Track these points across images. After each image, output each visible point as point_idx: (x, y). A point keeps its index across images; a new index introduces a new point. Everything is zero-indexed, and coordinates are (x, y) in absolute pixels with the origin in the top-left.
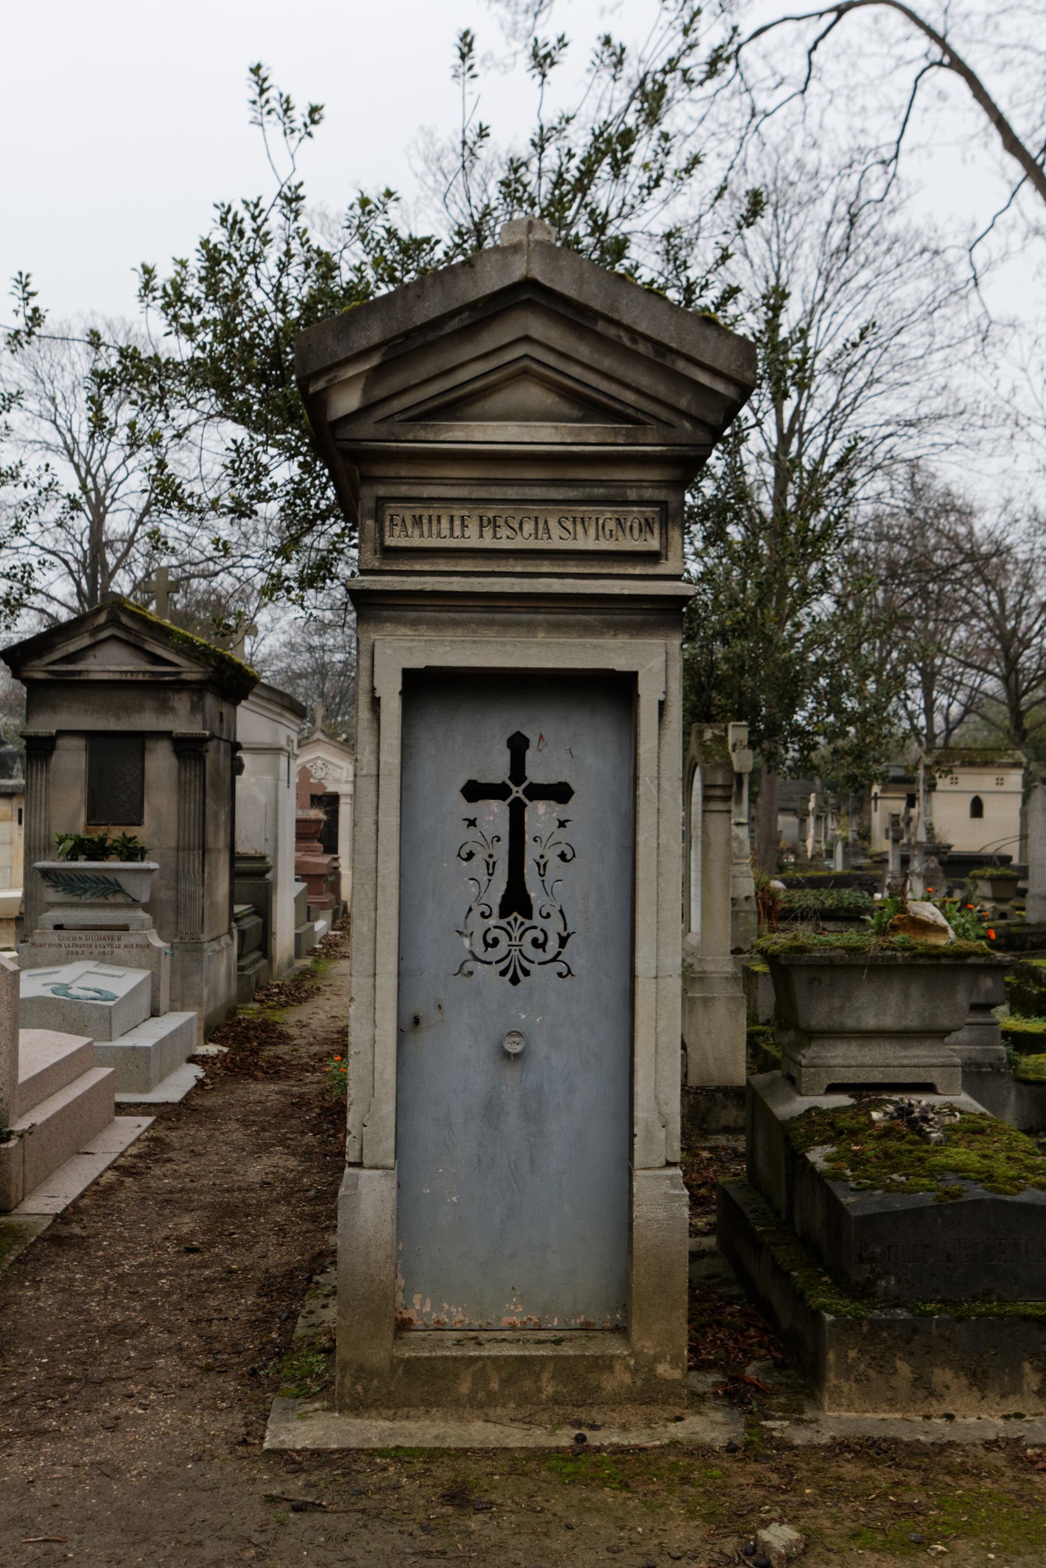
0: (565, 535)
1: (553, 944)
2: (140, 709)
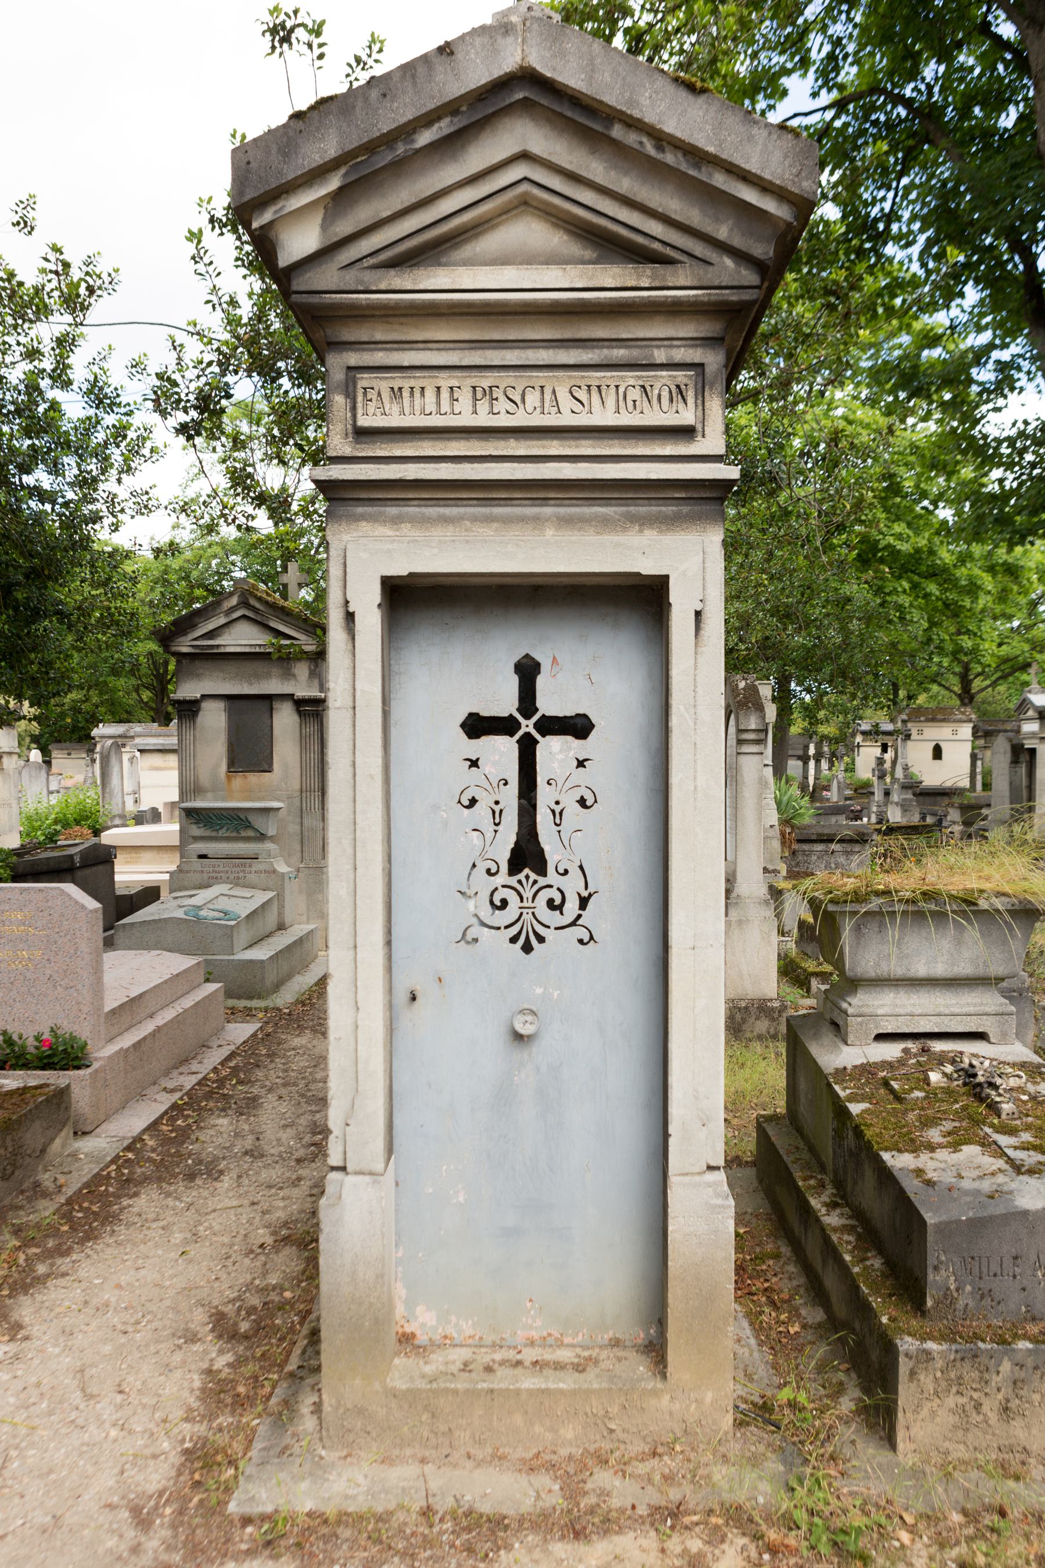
0: (578, 407)
1: (572, 907)
2: (268, 676)
